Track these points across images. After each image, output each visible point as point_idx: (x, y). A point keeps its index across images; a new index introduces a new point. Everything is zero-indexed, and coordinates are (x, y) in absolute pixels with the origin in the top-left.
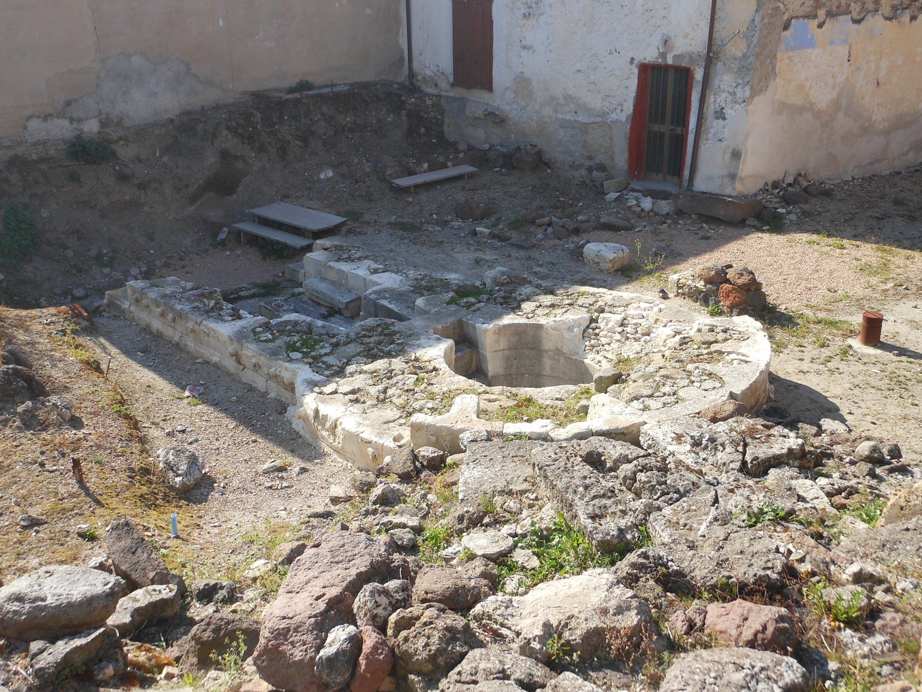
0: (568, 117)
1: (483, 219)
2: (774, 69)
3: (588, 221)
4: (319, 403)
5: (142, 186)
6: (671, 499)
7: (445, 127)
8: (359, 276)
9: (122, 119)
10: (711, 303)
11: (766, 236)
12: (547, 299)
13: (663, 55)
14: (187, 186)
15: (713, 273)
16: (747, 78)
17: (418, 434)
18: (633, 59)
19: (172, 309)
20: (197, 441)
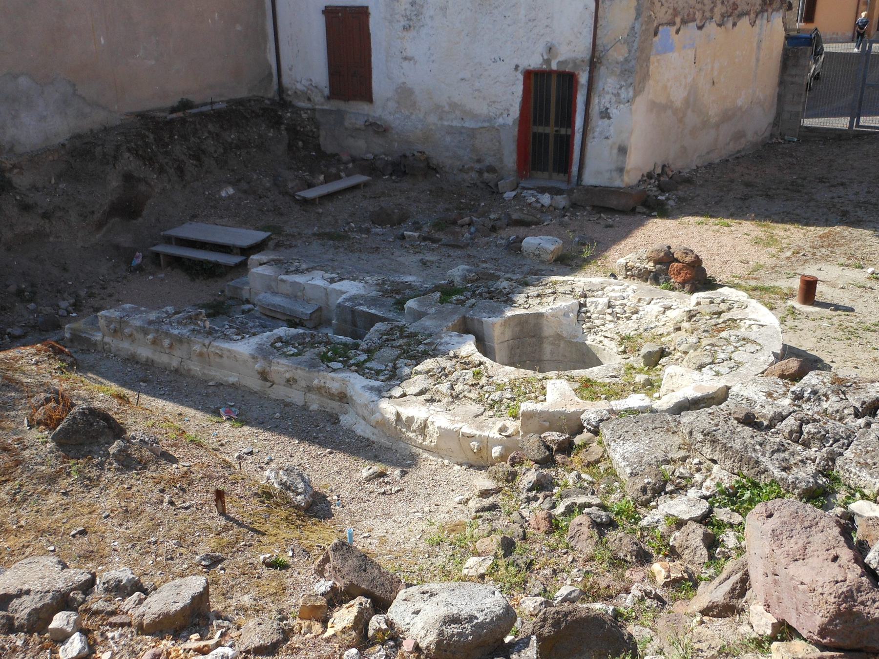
0: (455, 124)
1: (400, 224)
2: (648, 71)
3: (499, 219)
4: (397, 407)
5: (46, 216)
6: (844, 444)
7: (321, 139)
8: (319, 287)
9: (13, 146)
10: (661, 281)
11: (659, 221)
12: (532, 291)
13: (548, 62)
14: (93, 212)
15: (662, 254)
16: (630, 81)
17: (529, 422)
18: (517, 67)
19: (167, 334)
20: (271, 460)
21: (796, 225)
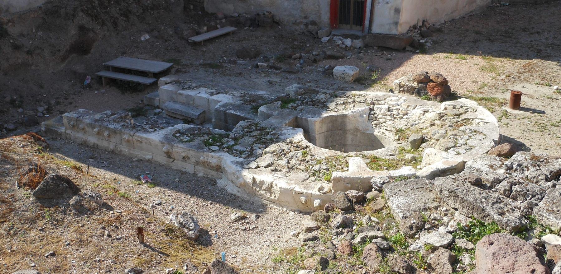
1: (255, 58)
3: (319, 55)
5: (29, 53)
6: (538, 198)
7: (205, 4)
9: (8, 8)
12: (340, 101)
15: (423, 77)
19: (107, 128)
20: (173, 208)
21: (508, 59)
